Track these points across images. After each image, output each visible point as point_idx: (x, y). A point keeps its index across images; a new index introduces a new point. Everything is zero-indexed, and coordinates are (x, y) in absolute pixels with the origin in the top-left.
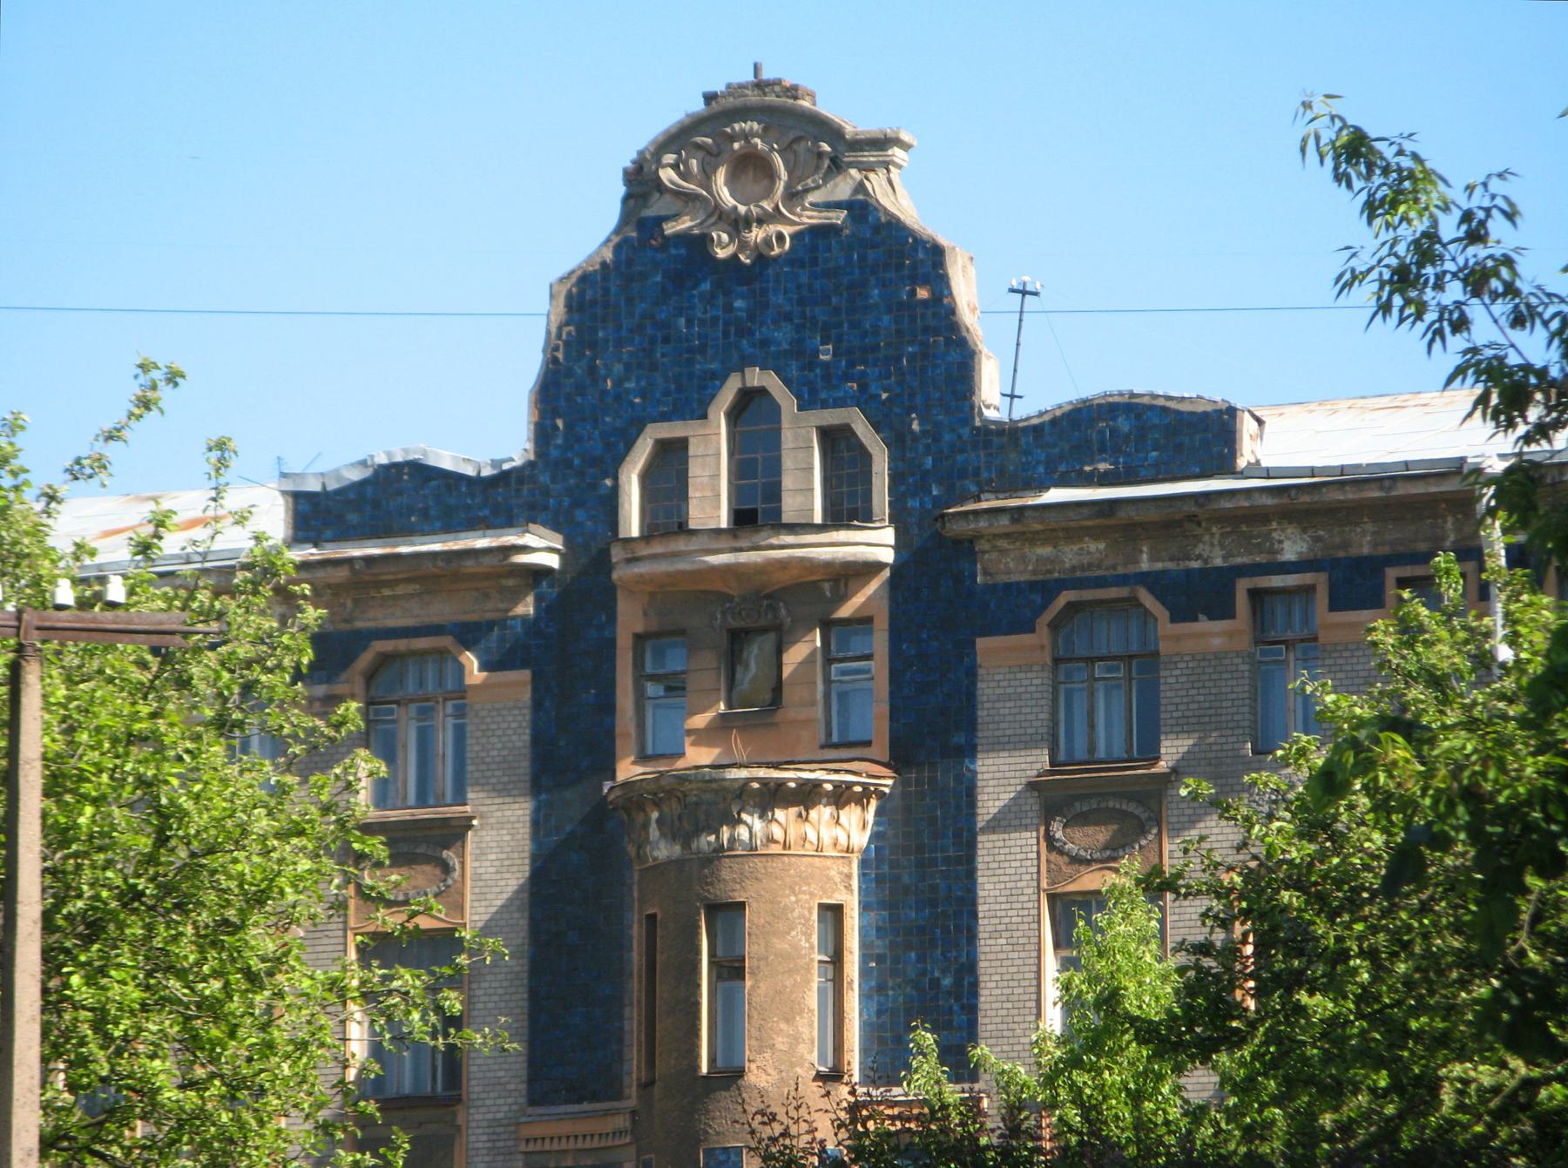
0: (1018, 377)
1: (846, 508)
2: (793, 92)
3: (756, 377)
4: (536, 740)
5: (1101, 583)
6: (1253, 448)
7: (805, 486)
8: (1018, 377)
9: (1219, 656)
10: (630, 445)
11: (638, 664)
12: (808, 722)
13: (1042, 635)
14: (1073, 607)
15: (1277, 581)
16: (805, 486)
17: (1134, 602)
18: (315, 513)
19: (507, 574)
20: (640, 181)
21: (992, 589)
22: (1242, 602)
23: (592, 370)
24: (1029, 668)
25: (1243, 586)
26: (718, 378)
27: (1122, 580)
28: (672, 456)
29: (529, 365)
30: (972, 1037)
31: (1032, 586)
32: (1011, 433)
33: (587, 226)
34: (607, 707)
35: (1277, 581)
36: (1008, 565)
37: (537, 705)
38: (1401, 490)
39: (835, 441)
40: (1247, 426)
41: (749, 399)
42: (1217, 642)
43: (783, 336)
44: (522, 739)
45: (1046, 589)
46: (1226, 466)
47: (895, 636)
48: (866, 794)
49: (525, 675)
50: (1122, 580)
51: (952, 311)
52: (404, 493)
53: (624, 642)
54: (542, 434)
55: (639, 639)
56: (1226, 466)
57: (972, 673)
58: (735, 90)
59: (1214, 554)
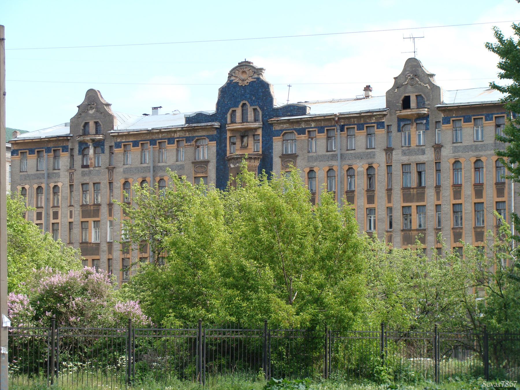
0: (280, 100)
1: (256, 120)
2: (250, 63)
3: (244, 102)
4: (217, 151)
5: (289, 130)
6: (308, 111)
7: (251, 116)
8: (280, 100)
9: (304, 140)
10: (229, 111)
11: (230, 140)
12: (251, 149)
13: (281, 137)
14: (285, 133)
15: (311, 130)
16: (251, 116)
17: (293, 132)
18: (189, 120)
19: (212, 128)
20: (230, 75)
21: (275, 130)
22: (307, 132)
23: (224, 101)
24: (279, 141)
25: (307, 130)
26: (239, 102)
27: (292, 129)
28: (234, 111)
29: (7, 43)
30: (272, 170)
31: (280, 130)
32: (278, 109)
33: (223, 81)
34: (226, 146)
35: (311, 130)
36: (277, 128)
37: (217, 146)
38: (326, 117)
39: (255, 110)
40: (308, 109)
41: (244, 105)
42: (303, 138)
43: (248, 96)
44: (215, 151)
45: (282, 131)
46: (305, 114)
47: (262, 137)
48: (258, 158)
49: (215, 142)
50: (292, 129)
51: (270, 92)
52: (200, 117)
53: (228, 138)
54: (217, 109)
55: (230, 137)
56: (305, 114)
57: (272, 142)
58: (242, 62)
59: (303, 126)
